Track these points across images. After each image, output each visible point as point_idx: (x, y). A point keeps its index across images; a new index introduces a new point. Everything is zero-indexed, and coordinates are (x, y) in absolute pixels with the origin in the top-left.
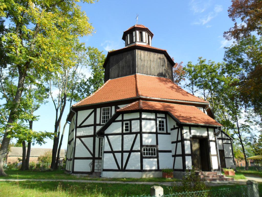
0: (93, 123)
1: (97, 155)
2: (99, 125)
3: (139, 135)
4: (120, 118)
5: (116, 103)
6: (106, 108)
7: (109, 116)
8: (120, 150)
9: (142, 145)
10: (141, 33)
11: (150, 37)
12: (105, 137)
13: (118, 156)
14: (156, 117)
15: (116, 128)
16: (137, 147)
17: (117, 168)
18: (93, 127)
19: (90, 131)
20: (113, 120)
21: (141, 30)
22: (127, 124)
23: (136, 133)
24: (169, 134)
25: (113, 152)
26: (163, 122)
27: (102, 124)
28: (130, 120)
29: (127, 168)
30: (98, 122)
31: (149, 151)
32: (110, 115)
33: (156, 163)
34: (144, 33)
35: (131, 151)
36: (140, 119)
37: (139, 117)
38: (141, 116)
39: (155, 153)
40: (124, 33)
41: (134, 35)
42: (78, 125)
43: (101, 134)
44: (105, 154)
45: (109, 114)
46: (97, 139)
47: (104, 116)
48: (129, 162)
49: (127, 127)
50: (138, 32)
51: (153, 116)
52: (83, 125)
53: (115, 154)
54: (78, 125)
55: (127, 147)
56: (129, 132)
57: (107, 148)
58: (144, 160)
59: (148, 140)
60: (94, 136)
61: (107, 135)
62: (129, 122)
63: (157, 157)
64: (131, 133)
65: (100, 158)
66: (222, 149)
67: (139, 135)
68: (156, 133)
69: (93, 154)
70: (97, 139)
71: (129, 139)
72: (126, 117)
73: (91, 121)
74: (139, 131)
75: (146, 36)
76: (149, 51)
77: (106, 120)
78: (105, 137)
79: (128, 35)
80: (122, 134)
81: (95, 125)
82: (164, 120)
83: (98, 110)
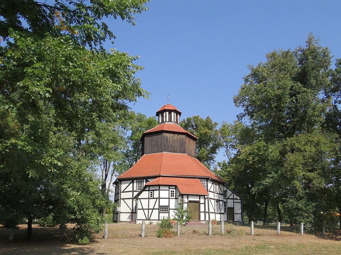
0: (132, 190)
1: (134, 211)
2: (136, 191)
3: (158, 199)
4: (147, 189)
5: (147, 178)
6: (140, 180)
7: (142, 186)
8: (148, 208)
9: (159, 206)
10: (170, 113)
11: (178, 115)
12: (139, 200)
13: (146, 211)
14: (169, 188)
15: (145, 194)
16: (157, 206)
17: (145, 219)
18: (132, 192)
19: (130, 195)
20: (144, 190)
21: (170, 111)
22: (151, 193)
23: (157, 198)
24: (178, 199)
25: (143, 209)
26: (173, 191)
27: (137, 190)
28: (153, 190)
29: (150, 219)
30: (135, 190)
31: (164, 209)
32: (142, 185)
33: (237, 213)
34: (173, 113)
35: (154, 209)
36: (159, 190)
37: (158, 189)
38: (159, 188)
39: (167, 210)
40: (157, 112)
41: (164, 115)
42: (122, 191)
43: (136, 198)
44: (138, 210)
46: (134, 202)
47: (141, 185)
48: (152, 215)
49: (151, 194)
50: (167, 113)
51: (167, 188)
52: (125, 191)
53: (144, 210)
54: (122, 191)
55: (151, 207)
56: (152, 197)
57: (139, 207)
58: (160, 214)
59: (164, 203)
60: (133, 199)
61: (140, 199)
62: (150, 197)
63: (169, 213)
64: (153, 198)
65: (136, 213)
66: (233, 207)
67: (158, 199)
68: (169, 199)
69: (132, 211)
70: (134, 202)
71: (152, 201)
72: (151, 188)
73: (130, 188)
74: (158, 197)
75: (174, 116)
76: (173, 134)
77: (140, 188)
78: (139, 200)
79: (160, 115)
80: (149, 198)
81: (133, 191)
82: (175, 190)
83: (135, 181)
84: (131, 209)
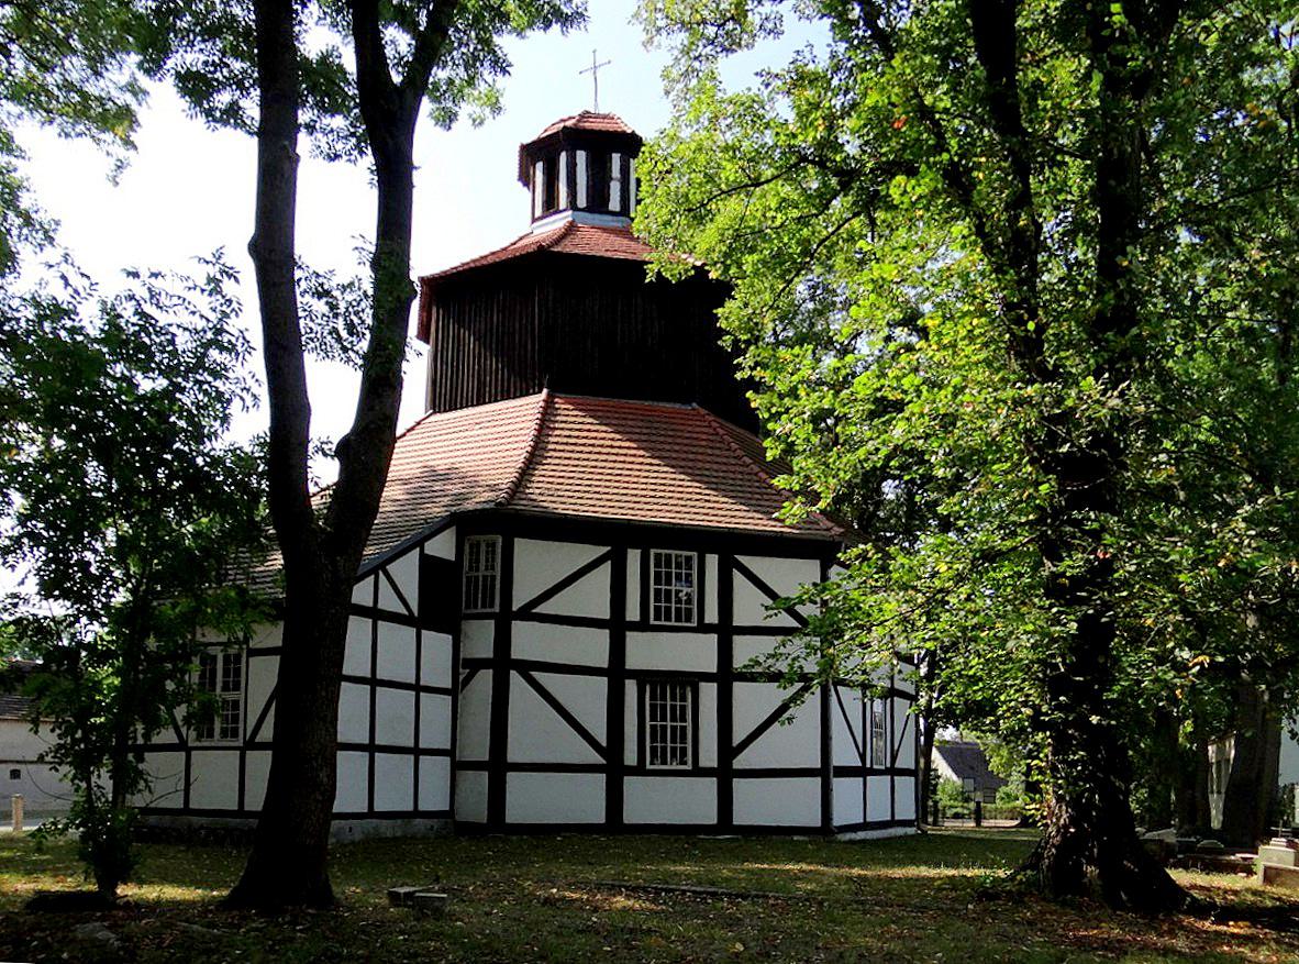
45: (658, 592)
84: (602, 737)
